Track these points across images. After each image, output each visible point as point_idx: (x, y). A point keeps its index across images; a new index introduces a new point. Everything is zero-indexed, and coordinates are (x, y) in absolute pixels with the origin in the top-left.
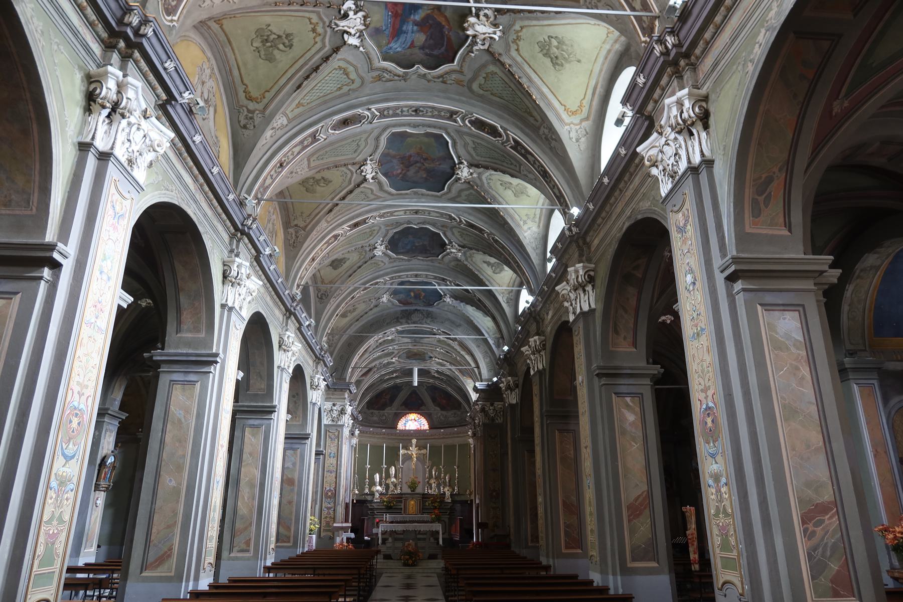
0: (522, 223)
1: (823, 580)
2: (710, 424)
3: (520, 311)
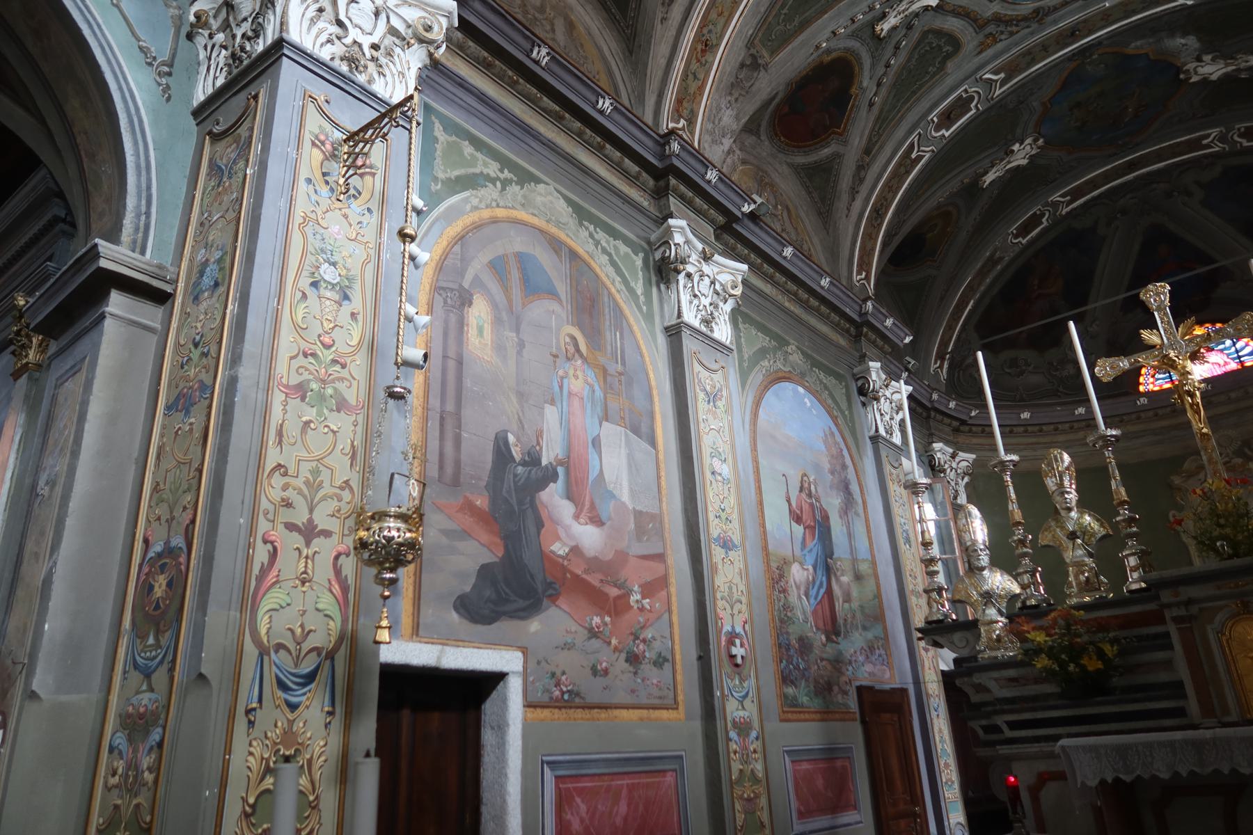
2: (159, 590)
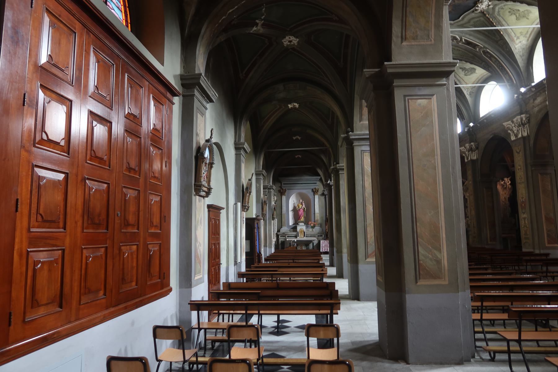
0: (515, 38)
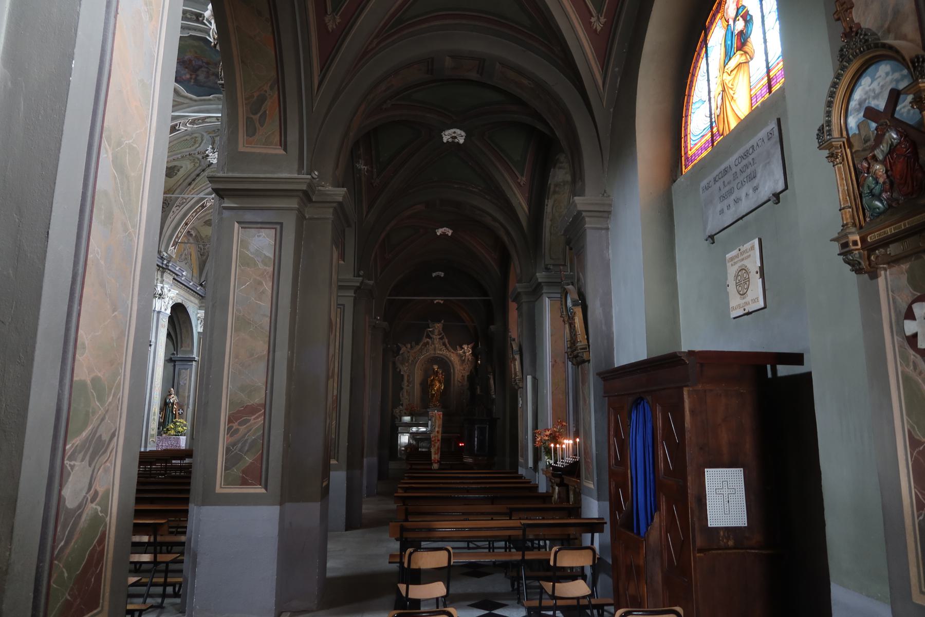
1: (236, 471)
3: (524, 223)
